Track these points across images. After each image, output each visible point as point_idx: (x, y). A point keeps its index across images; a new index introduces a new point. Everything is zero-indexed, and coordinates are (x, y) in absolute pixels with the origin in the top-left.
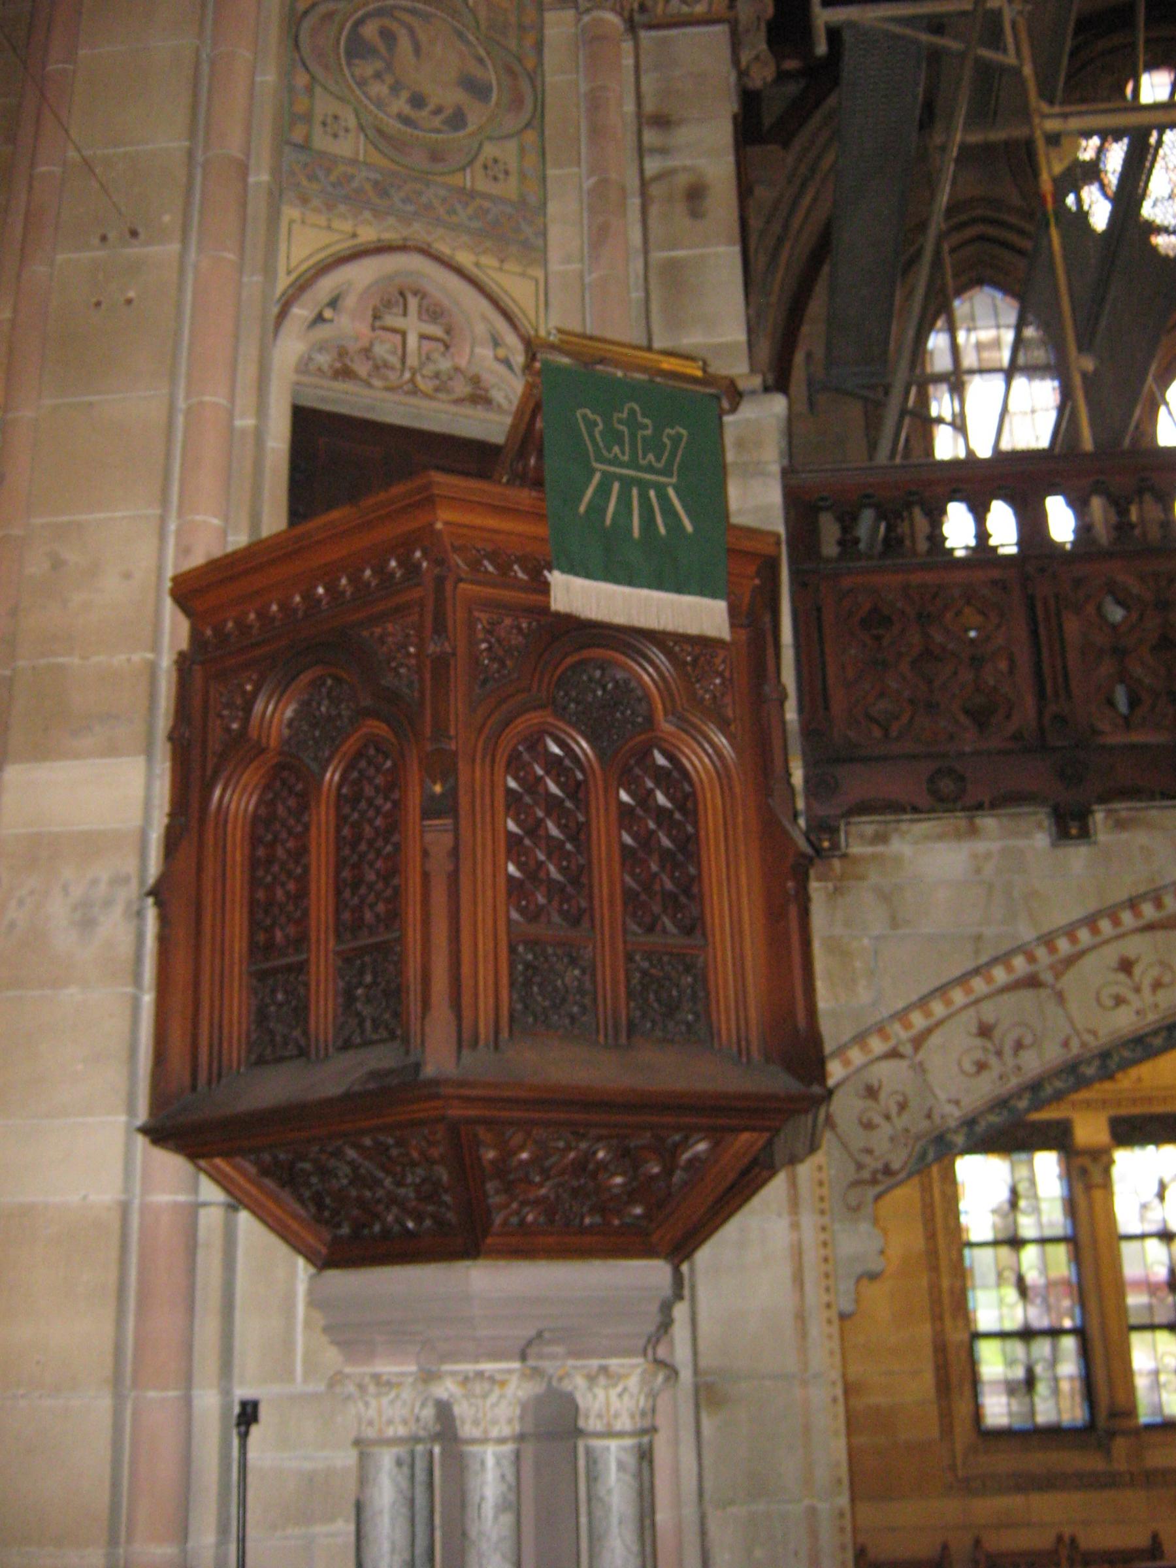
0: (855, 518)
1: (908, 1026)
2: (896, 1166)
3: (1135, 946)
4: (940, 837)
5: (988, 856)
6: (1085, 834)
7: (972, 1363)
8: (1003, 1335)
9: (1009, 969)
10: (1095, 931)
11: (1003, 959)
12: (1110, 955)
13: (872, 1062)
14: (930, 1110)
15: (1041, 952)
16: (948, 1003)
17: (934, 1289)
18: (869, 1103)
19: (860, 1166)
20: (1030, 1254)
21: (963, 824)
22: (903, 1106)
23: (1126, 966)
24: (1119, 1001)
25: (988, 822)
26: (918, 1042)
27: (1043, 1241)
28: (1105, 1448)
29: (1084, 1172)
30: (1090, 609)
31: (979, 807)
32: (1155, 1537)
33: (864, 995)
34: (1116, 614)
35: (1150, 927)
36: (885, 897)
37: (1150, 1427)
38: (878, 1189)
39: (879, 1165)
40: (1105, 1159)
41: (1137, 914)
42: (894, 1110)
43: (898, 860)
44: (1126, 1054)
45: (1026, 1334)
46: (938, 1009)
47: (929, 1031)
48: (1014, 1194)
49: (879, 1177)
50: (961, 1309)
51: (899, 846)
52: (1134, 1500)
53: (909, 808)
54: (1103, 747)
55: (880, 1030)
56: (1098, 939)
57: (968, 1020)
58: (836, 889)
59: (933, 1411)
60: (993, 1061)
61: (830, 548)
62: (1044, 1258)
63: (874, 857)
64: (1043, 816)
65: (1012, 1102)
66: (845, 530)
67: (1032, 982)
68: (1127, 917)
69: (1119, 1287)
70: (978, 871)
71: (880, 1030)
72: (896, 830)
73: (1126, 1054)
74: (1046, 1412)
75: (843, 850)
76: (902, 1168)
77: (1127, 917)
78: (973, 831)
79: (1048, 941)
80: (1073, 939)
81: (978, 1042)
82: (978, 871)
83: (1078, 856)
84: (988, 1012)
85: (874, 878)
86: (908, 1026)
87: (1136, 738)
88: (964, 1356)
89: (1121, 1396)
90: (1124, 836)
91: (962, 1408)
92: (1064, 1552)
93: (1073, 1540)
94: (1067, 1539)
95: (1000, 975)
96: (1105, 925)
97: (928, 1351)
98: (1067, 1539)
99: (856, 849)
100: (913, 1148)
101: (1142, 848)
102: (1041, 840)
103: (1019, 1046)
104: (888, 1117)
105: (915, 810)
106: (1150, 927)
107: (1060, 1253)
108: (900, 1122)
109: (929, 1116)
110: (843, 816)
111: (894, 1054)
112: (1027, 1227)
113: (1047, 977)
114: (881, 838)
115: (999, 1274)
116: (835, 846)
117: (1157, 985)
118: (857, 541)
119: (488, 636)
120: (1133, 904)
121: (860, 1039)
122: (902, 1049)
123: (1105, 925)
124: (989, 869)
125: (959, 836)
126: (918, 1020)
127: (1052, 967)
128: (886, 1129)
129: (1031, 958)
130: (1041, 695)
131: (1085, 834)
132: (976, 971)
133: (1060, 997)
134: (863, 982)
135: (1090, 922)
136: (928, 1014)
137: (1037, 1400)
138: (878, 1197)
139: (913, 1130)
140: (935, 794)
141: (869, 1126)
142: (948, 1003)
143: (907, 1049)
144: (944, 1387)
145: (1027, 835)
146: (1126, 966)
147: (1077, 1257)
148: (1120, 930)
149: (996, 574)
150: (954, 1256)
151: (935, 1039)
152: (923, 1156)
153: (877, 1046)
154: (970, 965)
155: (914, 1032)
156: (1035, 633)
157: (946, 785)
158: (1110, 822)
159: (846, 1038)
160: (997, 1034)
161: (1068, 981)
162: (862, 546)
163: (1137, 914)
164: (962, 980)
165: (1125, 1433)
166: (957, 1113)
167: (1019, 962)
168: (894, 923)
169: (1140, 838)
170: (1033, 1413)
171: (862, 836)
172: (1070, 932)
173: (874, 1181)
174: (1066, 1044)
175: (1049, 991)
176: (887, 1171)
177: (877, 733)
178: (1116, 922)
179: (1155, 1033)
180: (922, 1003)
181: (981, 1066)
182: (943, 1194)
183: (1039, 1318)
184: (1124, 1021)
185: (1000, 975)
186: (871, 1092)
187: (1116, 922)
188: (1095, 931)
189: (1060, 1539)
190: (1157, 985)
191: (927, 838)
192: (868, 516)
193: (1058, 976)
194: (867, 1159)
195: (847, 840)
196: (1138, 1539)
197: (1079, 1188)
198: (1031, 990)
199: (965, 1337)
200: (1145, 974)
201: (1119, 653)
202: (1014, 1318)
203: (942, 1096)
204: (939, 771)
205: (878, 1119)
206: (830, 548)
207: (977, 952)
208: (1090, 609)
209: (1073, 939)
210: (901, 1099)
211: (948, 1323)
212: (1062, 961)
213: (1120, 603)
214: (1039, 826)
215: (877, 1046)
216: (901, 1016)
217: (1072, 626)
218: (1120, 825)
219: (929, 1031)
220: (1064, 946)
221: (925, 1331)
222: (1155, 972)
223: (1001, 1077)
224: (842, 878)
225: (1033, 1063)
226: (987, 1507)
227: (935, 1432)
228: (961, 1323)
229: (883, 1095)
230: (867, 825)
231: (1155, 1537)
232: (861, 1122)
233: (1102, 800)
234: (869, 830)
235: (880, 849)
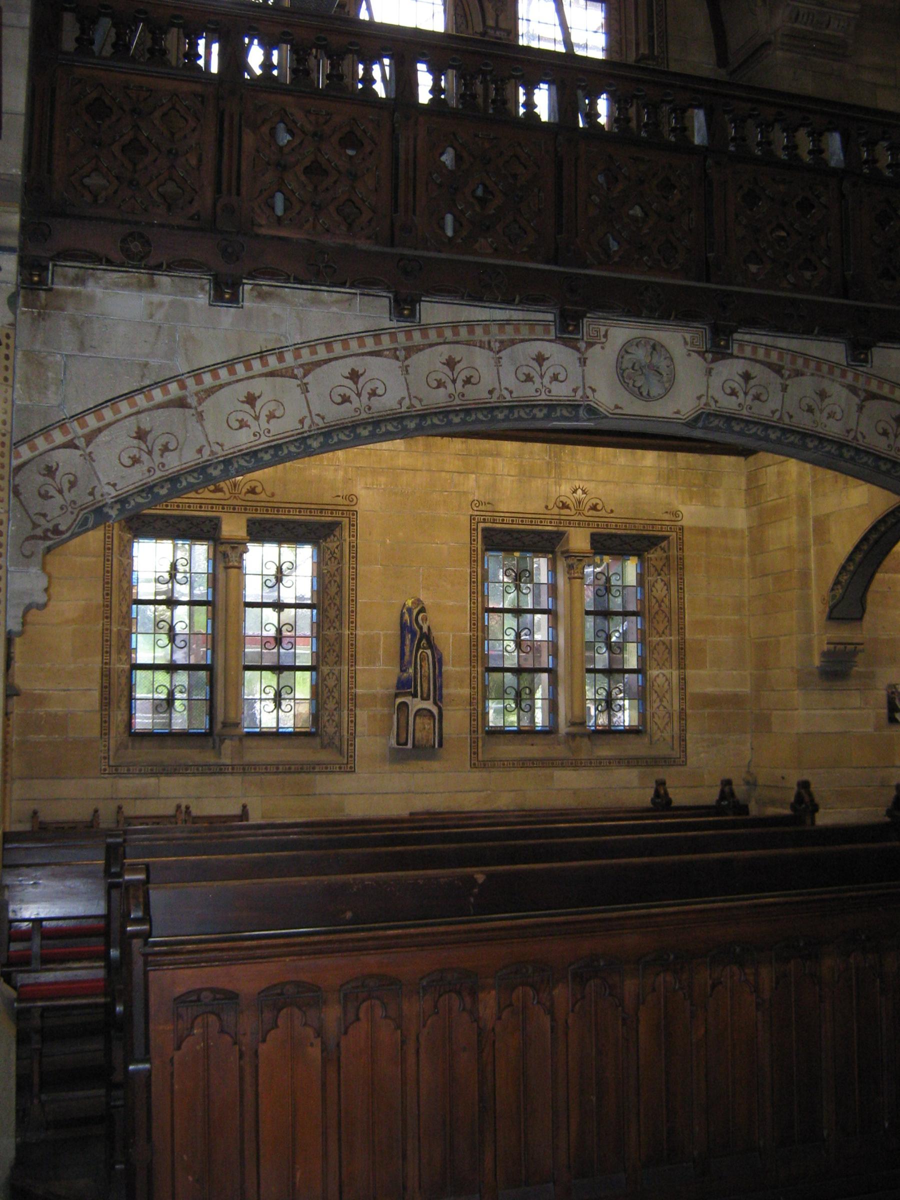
0: (94, 22)
1: (83, 425)
2: (62, 528)
3: (259, 386)
4: (126, 286)
5: (161, 304)
6: (235, 300)
7: (130, 687)
8: (154, 667)
9: (166, 392)
10: (232, 372)
11: (162, 384)
12: (242, 389)
13: (53, 449)
14: (94, 488)
15: (190, 382)
16: (117, 411)
17: (106, 631)
18: (49, 480)
19: (35, 526)
20: (182, 612)
21: (145, 278)
22: (73, 484)
23: (251, 400)
24: (243, 424)
25: (164, 280)
26: (90, 438)
27: (192, 603)
28: (217, 749)
29: (225, 555)
30: (265, 129)
31: (159, 267)
32: (244, 807)
33: (52, 398)
34: (284, 138)
35: (272, 374)
36: (78, 326)
37: (249, 734)
38: (48, 543)
39: (50, 526)
40: (241, 547)
41: (265, 364)
42: (66, 486)
43: (91, 299)
44: (242, 462)
45: (171, 668)
46: (108, 414)
47: (100, 430)
48: (174, 567)
49: (49, 534)
50: (127, 648)
51: (92, 288)
52: (233, 782)
53: (104, 260)
54: (257, 235)
55: (61, 425)
56: (234, 378)
57: (131, 425)
58: (39, 314)
59: (97, 718)
60: (145, 457)
61: (69, 44)
62: (191, 616)
63: (73, 294)
64: (206, 282)
65: (156, 490)
66: (83, 31)
67: (181, 403)
68: (257, 365)
69: (241, 639)
70: (151, 316)
71: (61, 425)
72: (92, 275)
73: (242, 462)
74: (180, 720)
75: (50, 285)
76: (67, 531)
77: (257, 365)
78: (152, 285)
79: (196, 374)
80: (216, 376)
81: (136, 442)
82: (151, 316)
83: (227, 315)
84: (146, 421)
85: (70, 310)
86: (83, 425)
87: (284, 233)
88: (123, 680)
89: (232, 715)
90: (264, 305)
91: (119, 716)
92: (183, 816)
93: (187, 808)
94: (183, 809)
95: (158, 395)
96: (240, 368)
97: (97, 676)
98: (183, 809)
99: (59, 286)
100: (78, 516)
101: (275, 315)
102: (202, 299)
103: (165, 449)
104: (60, 491)
105: (109, 262)
106: (272, 374)
107: (201, 613)
108: (69, 496)
109: (92, 494)
110: (52, 259)
111: (70, 445)
112: (182, 592)
113: (192, 401)
114: (80, 280)
115: (157, 624)
116: (43, 281)
117: (271, 416)
118: (92, 42)
119: (167, 304)
120: (262, 355)
121: (45, 431)
122: (77, 442)
123: (240, 368)
124: (159, 315)
125: (140, 287)
126: (92, 422)
127: (196, 394)
128: (58, 500)
129: (183, 386)
130: (218, 190)
131: (235, 300)
132: (140, 390)
133: (200, 416)
134: (53, 388)
135: (230, 364)
136: (100, 418)
137: (174, 715)
138: (49, 550)
139: (79, 503)
140: (126, 252)
141: (45, 496)
142: (117, 411)
143: (81, 442)
144: (106, 702)
145: (193, 294)
146: (251, 400)
147: (213, 617)
148: (250, 374)
149: (198, 88)
150: (124, 609)
151: (103, 437)
152: (86, 520)
153: (59, 437)
154: (136, 386)
155: (86, 430)
156: (220, 141)
157: (135, 246)
158: (255, 293)
159: (35, 429)
160: (150, 438)
161: (207, 405)
162: (96, 48)
163: (265, 364)
164: (128, 396)
165: (232, 737)
166: (114, 494)
167: (173, 387)
168: (82, 347)
169: (273, 307)
170: (170, 724)
171: (65, 277)
172: (213, 370)
173: (45, 538)
174: (200, 451)
175: (193, 411)
176: (56, 531)
177: (88, 198)
178: (249, 368)
179: (265, 450)
180: (96, 409)
181: (136, 461)
182: (121, 563)
183: (180, 657)
184: (244, 439)
185: (158, 395)
186: (50, 472)
187: (249, 368)
188: (232, 372)
189: (179, 807)
190: (271, 416)
191: (116, 285)
192: (106, 23)
193: (200, 401)
194: (42, 521)
195: (53, 279)
196: (236, 810)
197: (221, 566)
198: (327, 498)
199: (127, 667)
200: (264, 407)
201: (282, 167)
202: (162, 656)
203: (104, 480)
204: (131, 234)
205: (53, 492)
206: (69, 44)
207: (143, 376)
208: (265, 129)
209: (216, 376)
210: (72, 478)
211: (114, 656)
212: (205, 391)
213: (290, 131)
214: (202, 289)
215: (59, 437)
216: (79, 417)
217: (249, 140)
218: (262, 296)
219: (100, 430)
220: (208, 379)
221: (96, 662)
222: (272, 406)
223: (149, 471)
224: (46, 307)
225: (174, 463)
226: (128, 785)
227: (96, 732)
228: (124, 657)
229: (59, 474)
230: (70, 269)
231: (244, 807)
232: (40, 494)
233: (251, 276)
234: (71, 272)
235: (78, 288)
